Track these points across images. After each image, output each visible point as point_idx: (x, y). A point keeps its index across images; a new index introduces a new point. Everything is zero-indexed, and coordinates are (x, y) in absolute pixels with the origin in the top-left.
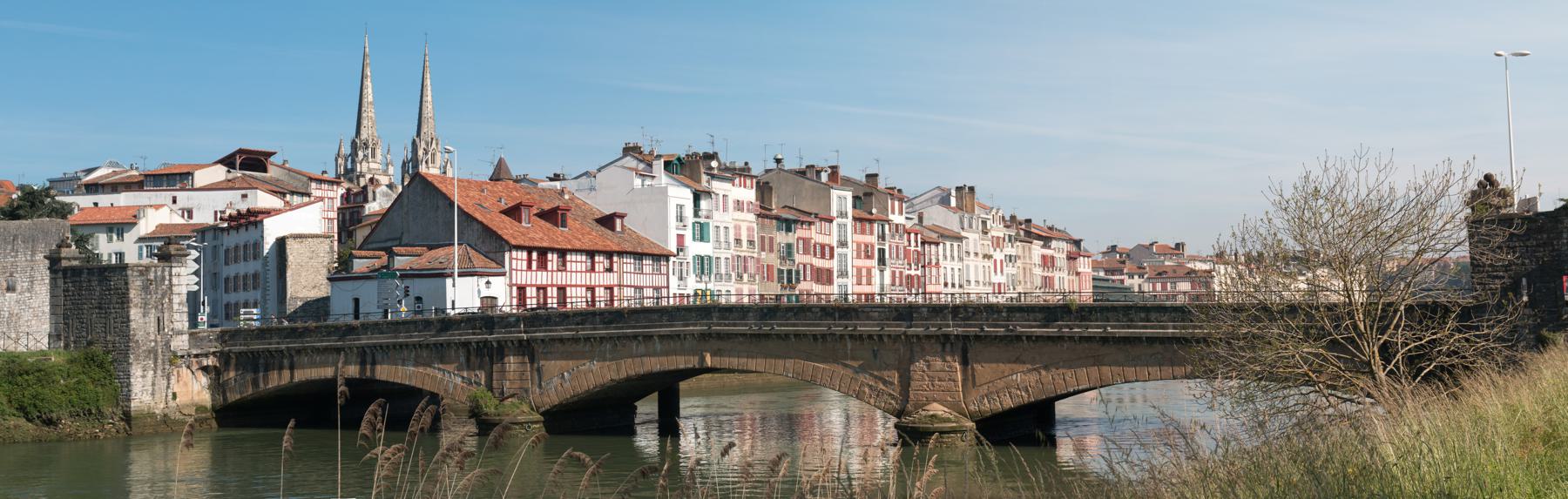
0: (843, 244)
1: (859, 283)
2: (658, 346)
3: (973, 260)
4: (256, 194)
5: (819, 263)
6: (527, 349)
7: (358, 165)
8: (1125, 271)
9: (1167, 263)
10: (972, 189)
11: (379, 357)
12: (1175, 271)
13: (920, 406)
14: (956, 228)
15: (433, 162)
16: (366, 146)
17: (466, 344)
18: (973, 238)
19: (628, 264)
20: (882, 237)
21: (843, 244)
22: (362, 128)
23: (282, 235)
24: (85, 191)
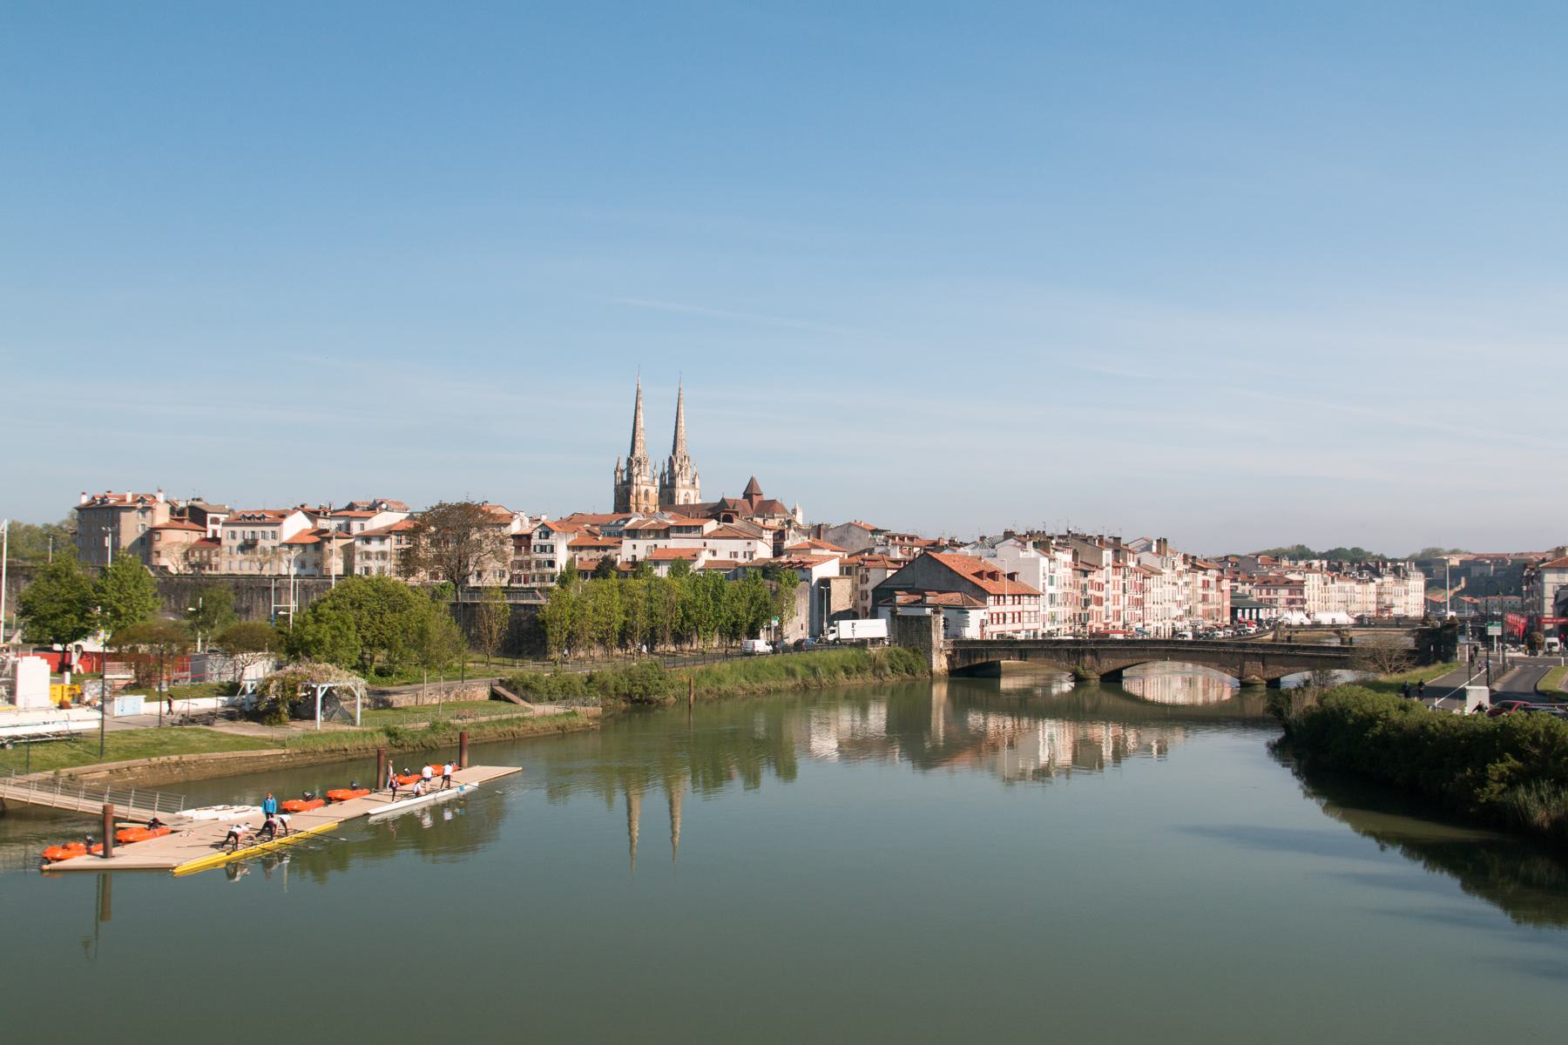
0: (1108, 582)
1: (1114, 605)
2: (1149, 653)
5: (1098, 594)
6: (1094, 653)
7: (635, 478)
8: (1239, 580)
9: (1270, 574)
10: (1165, 540)
11: (1028, 653)
13: (1247, 676)
14: (1159, 567)
15: (686, 475)
16: (639, 462)
17: (1068, 650)
18: (1167, 571)
19: (1025, 600)
20: (1124, 577)
21: (1108, 582)
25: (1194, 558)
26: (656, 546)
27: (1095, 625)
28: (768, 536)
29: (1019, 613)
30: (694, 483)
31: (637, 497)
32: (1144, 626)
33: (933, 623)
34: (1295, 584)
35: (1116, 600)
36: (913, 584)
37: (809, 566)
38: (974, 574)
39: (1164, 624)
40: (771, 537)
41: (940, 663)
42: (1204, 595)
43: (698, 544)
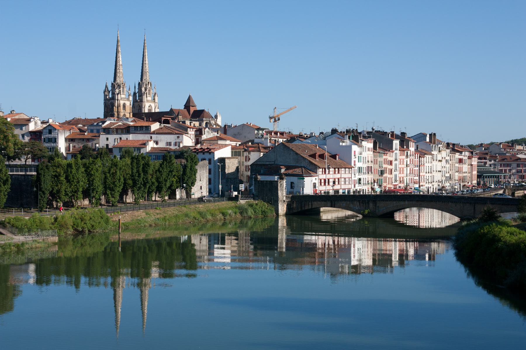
0: (396, 160)
4: (183, 136)
10: (435, 134)
12: (511, 159)
21: (396, 160)
22: (117, 77)
23: (225, 157)
24: (115, 133)
25: (454, 145)
26: (121, 138)
27: (388, 186)
28: (192, 132)
29: (339, 179)
30: (154, 99)
31: (118, 108)
32: (419, 186)
33: (279, 185)
34: (522, 160)
35: (401, 171)
36: (274, 162)
37: (212, 151)
38: (310, 156)
39: (433, 185)
40: (193, 133)
41: (282, 209)
43: (146, 137)
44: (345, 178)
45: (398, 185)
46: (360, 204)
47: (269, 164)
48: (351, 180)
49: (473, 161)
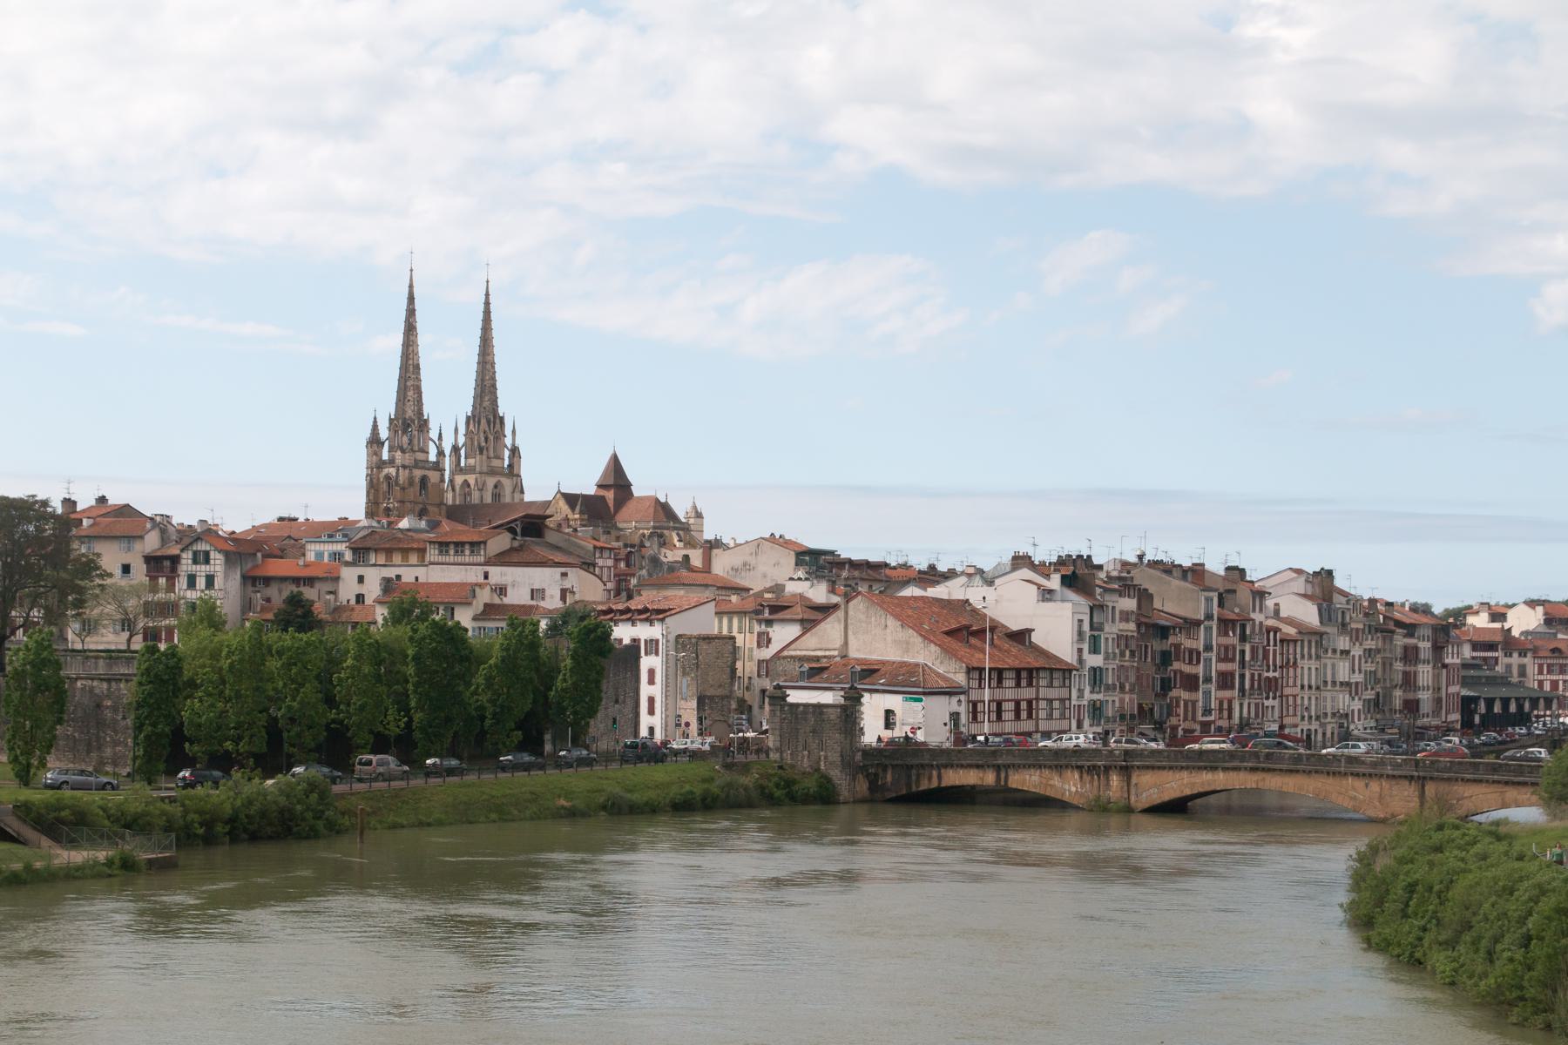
3: (1331, 658)
5: (1187, 669)
26: (398, 577)
29: (1030, 702)
39: (1323, 725)
42: (1406, 674)
43: (473, 575)
44: (1050, 701)
45: (1214, 722)
46: (1081, 777)
47: (825, 657)
48: (1067, 706)
49: (1450, 655)
